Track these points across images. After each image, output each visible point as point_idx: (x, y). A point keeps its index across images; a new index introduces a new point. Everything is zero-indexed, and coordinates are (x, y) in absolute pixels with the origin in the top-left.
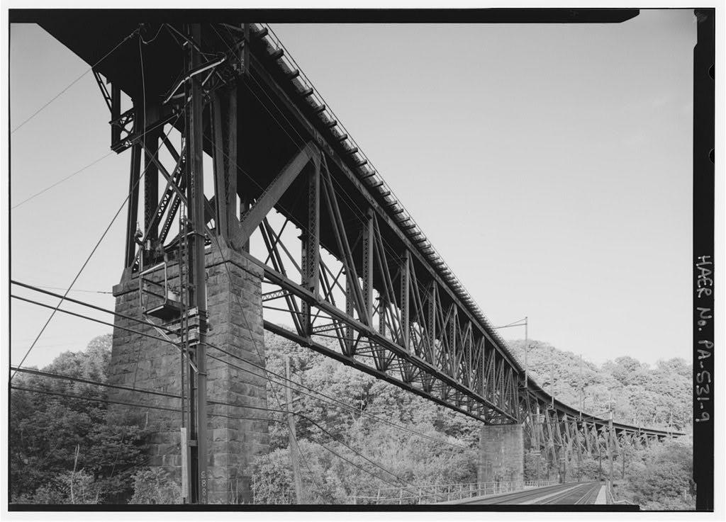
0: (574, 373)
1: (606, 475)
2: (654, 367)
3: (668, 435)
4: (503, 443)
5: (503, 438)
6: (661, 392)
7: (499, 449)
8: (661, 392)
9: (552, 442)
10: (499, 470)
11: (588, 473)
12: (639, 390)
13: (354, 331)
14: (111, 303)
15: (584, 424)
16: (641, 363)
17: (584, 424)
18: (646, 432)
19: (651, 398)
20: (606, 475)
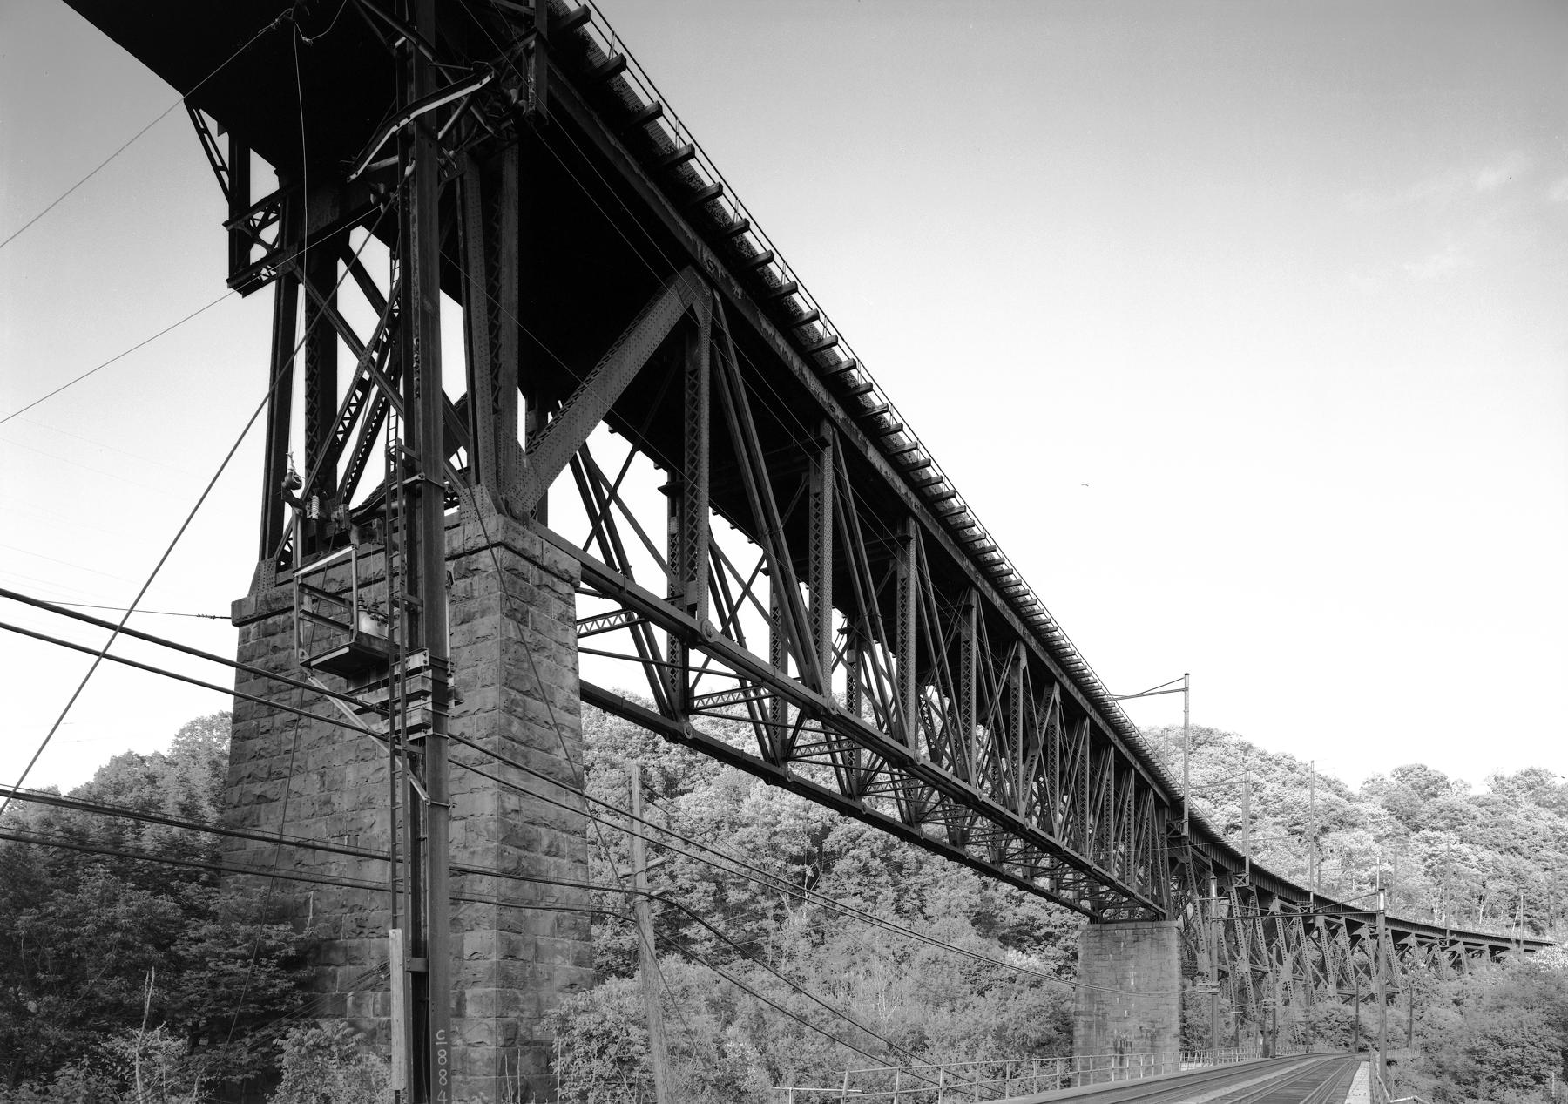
0: (1296, 803)
2: (1481, 789)
3: (1513, 946)
5: (1132, 952)
7: (1124, 978)
10: (1121, 1025)
11: (1329, 1033)
12: (1447, 842)
15: (1320, 921)
16: (1451, 780)
19: (1473, 860)
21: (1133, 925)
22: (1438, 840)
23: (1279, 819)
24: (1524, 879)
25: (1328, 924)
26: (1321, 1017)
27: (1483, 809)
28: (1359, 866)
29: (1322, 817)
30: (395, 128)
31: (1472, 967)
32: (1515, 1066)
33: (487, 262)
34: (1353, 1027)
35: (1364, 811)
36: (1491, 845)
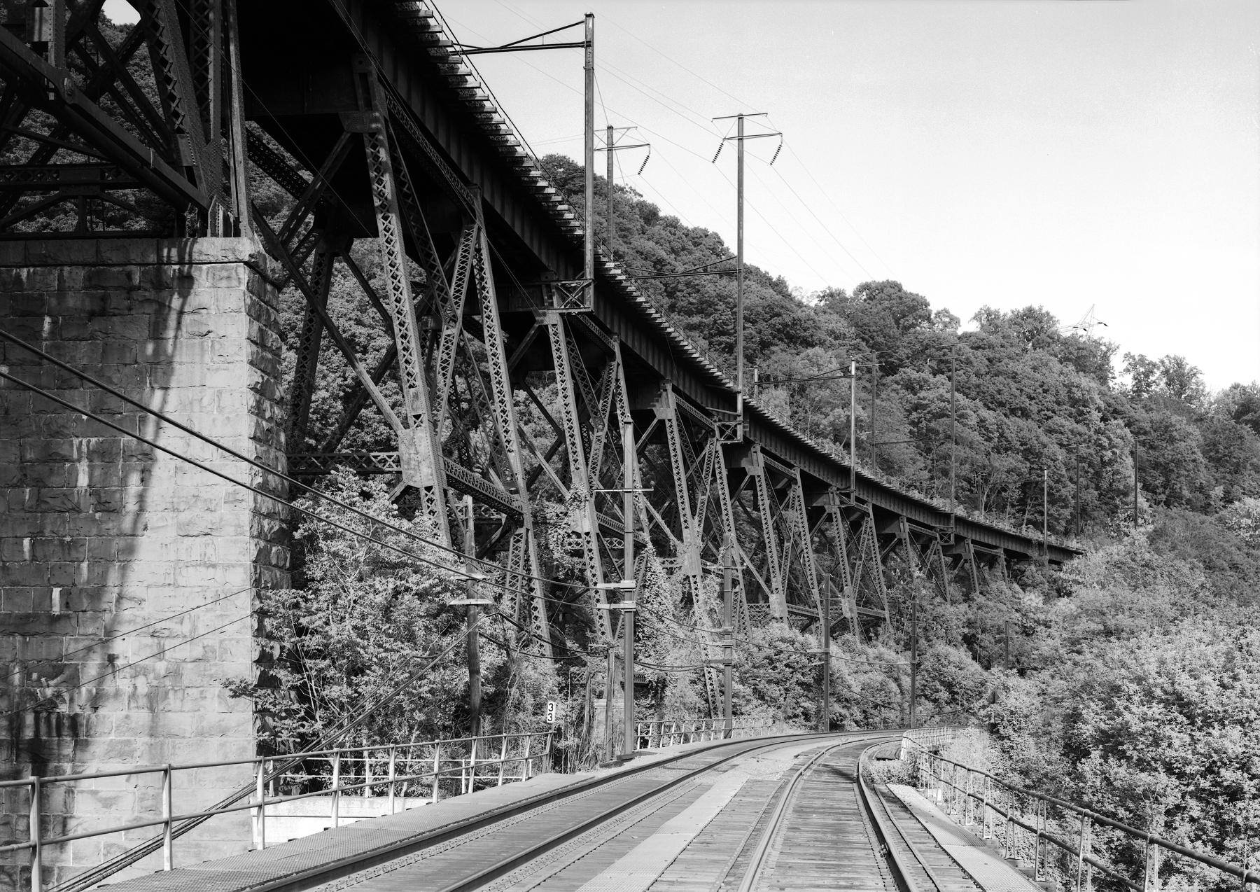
0: (721, 297)
1: (846, 702)
2: (969, 326)
3: (1034, 553)
4: (81, 398)
5: (82, 355)
6: (1001, 404)
7: (54, 459)
8: (1001, 404)
9: (589, 508)
10: (40, 649)
11: (775, 691)
12: (939, 390)
13: (51, 162)
14: (248, 448)
15: (756, 465)
16: (934, 308)
17: (756, 465)
18: (971, 535)
19: (973, 421)
20: (846, 702)
21: (86, 251)
22: (923, 385)
23: (696, 319)
24: (1039, 455)
25: (770, 472)
26: (759, 657)
27: (979, 353)
28: (817, 409)
29: (762, 325)
30: (293, 162)
31: (984, 582)
32: (1229, 776)
33: (196, 89)
34: (819, 680)
35: (825, 326)
36: (994, 403)
